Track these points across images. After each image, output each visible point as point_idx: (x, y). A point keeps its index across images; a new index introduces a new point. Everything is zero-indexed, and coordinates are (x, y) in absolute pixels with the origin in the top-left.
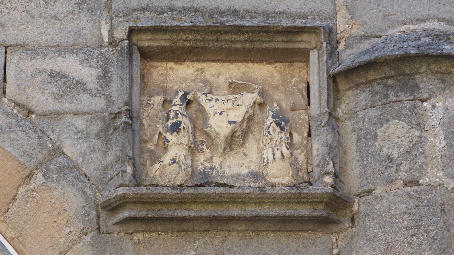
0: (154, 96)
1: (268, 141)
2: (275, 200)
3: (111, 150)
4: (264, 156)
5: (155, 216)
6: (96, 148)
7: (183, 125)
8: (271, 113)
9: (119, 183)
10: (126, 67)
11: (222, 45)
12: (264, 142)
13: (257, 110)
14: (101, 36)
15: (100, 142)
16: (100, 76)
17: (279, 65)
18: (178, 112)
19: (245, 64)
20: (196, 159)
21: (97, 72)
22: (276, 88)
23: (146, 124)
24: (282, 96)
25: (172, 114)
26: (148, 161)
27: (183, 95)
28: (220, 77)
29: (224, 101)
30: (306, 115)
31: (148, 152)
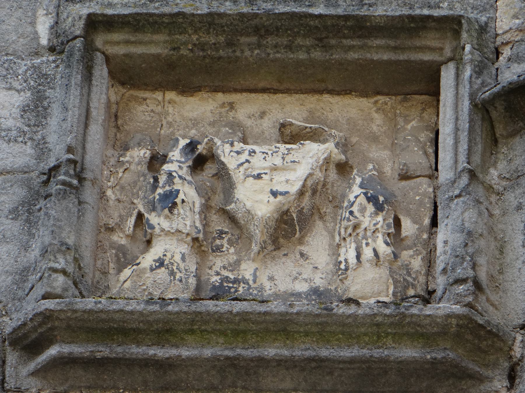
0: (133, 148)
1: (350, 230)
2: (349, 329)
3: (36, 237)
4: (342, 259)
5: (110, 356)
6: (8, 234)
7: (181, 196)
8: (358, 180)
9: (42, 292)
10: (76, 84)
11: (269, 54)
12: (343, 231)
13: (333, 175)
14: (36, 36)
15: (18, 224)
16: (28, 106)
17: (382, 99)
18: (174, 174)
19: (317, 97)
20: (209, 264)
21: (21, 98)
22: (374, 139)
23: (113, 197)
24: (385, 154)
25: (163, 178)
26: (112, 265)
27: (188, 145)
28: (266, 118)
29: (265, 155)
30: (430, 187)
31: (114, 248)
